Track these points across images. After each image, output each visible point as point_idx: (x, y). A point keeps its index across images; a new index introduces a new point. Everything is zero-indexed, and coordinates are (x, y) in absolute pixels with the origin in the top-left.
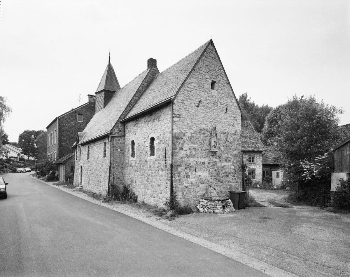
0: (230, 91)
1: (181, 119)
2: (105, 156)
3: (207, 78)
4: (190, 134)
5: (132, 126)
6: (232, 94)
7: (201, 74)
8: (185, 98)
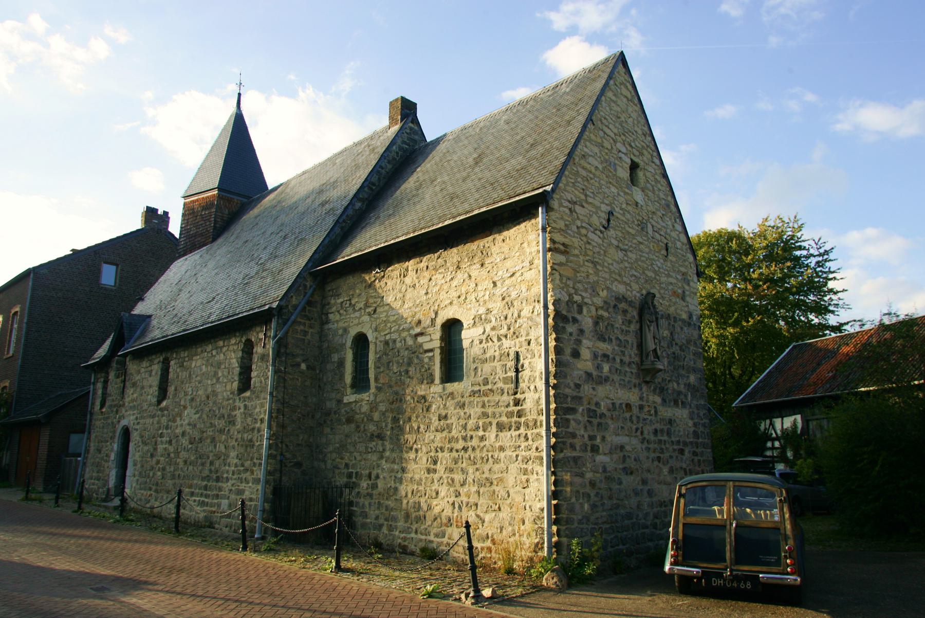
2: (245, 383)
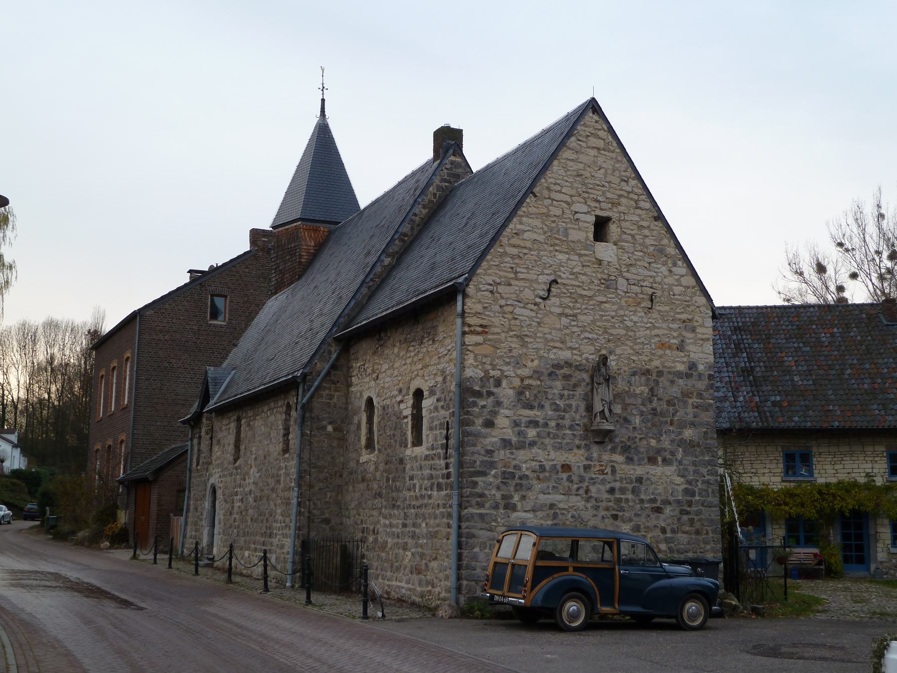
0: (665, 241)
1: (490, 337)
3: (576, 213)
4: (518, 380)
5: (370, 352)
6: (671, 250)
7: (557, 201)
8: (500, 277)
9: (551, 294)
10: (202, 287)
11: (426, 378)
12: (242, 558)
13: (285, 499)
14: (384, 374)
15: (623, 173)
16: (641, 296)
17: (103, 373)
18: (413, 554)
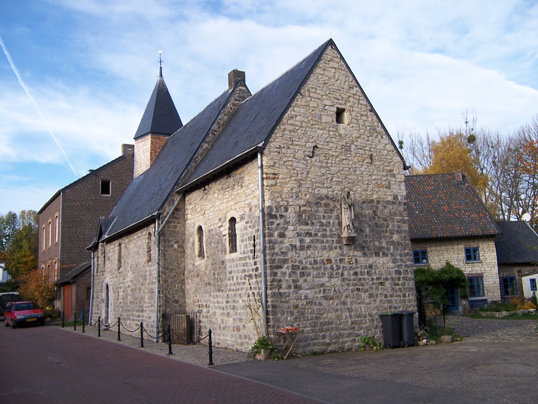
3: (325, 105)
6: (380, 129)
7: (314, 98)
9: (315, 154)
10: (96, 176)
11: (238, 210)
12: (126, 325)
13: (150, 289)
14: (208, 211)
15: (350, 83)
16: (365, 156)
17: (44, 226)
18: (234, 319)
